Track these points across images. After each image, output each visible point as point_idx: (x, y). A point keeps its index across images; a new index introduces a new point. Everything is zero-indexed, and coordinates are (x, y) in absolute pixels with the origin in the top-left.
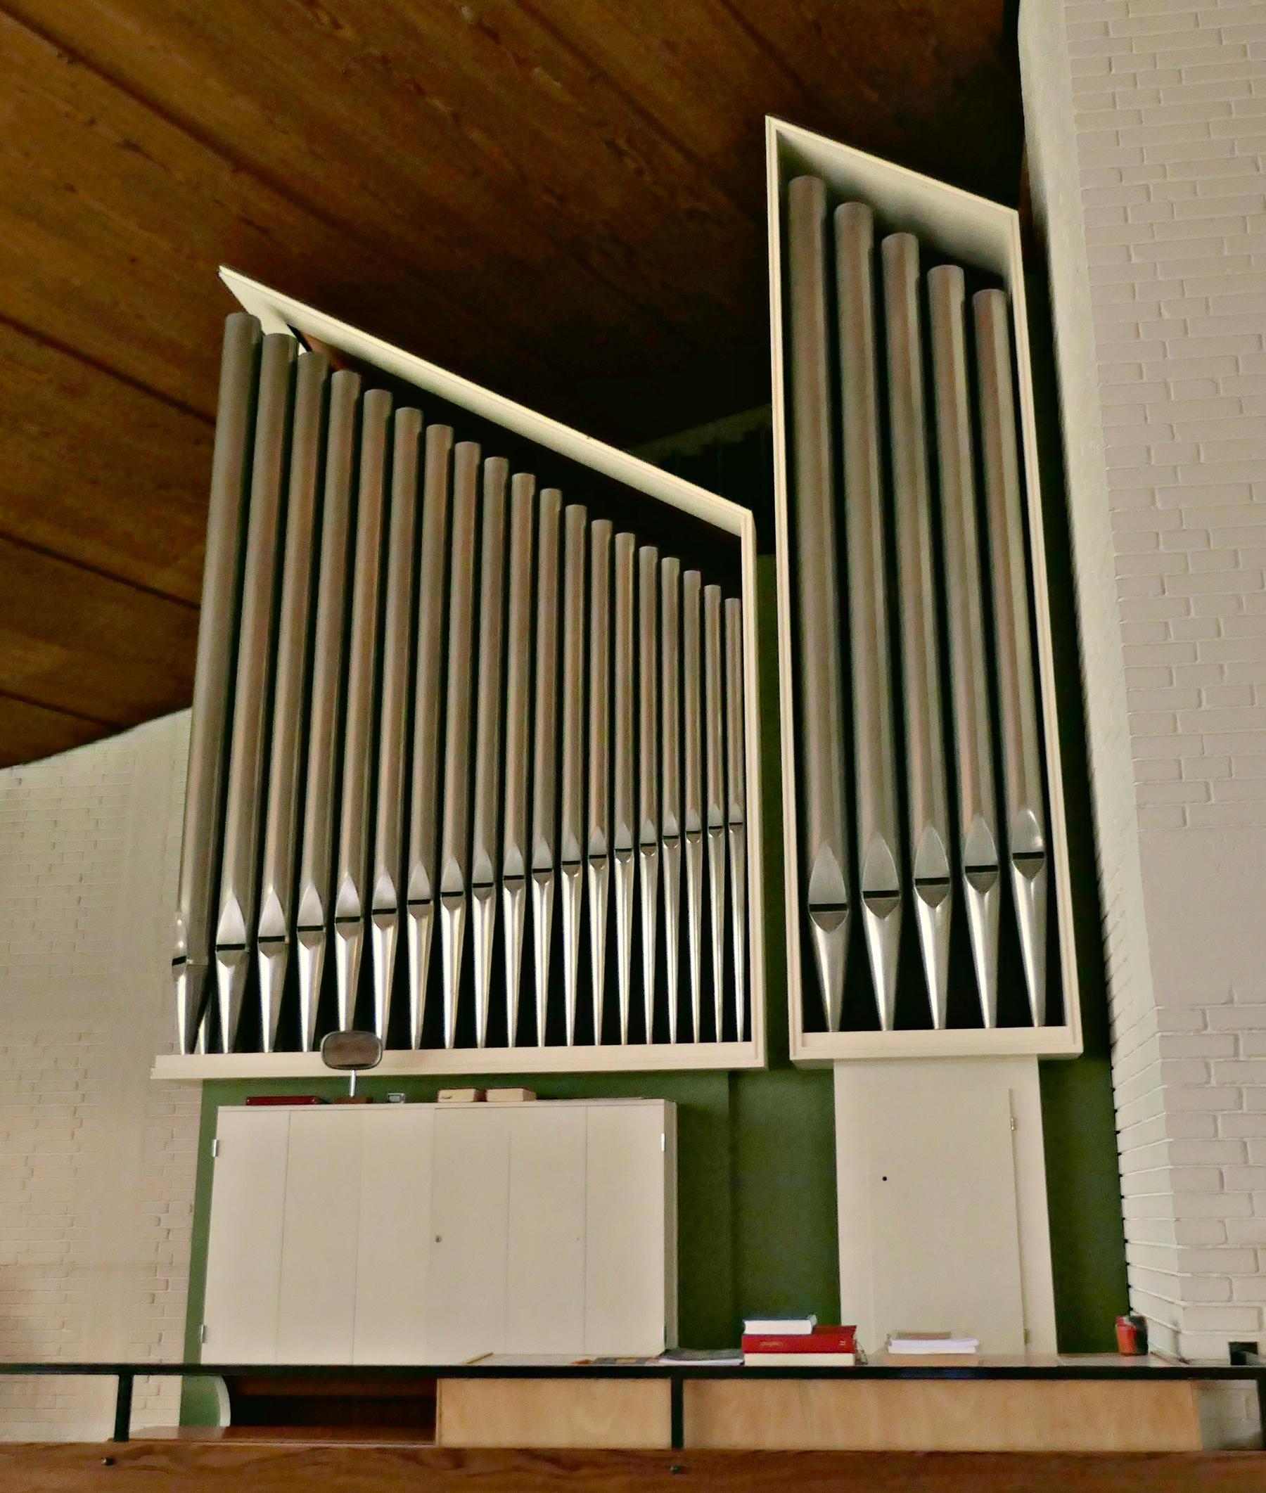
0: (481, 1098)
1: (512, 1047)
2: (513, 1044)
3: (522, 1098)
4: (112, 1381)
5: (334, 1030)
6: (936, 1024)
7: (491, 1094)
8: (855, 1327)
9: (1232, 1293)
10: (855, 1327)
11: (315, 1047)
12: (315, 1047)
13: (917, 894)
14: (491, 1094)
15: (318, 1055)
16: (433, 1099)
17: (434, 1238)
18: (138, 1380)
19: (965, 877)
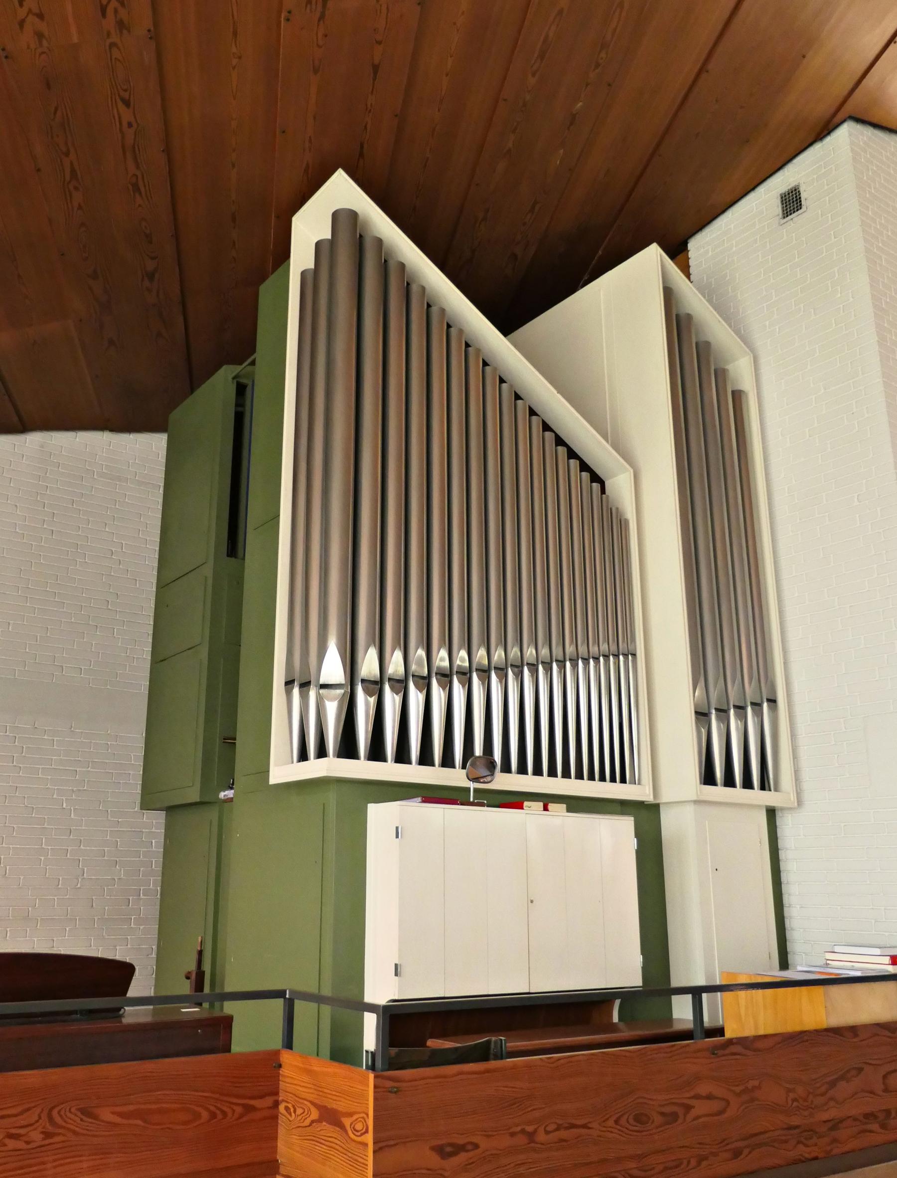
0: (546, 808)
1: (439, 767)
2: (416, 762)
3: (542, 809)
4: (689, 997)
5: (471, 757)
6: (596, 780)
7: (551, 806)
8: (292, 1050)
9: (630, 1125)
10: (292, 1050)
11: (464, 767)
12: (464, 767)
13: (411, 679)
14: (551, 806)
15: (464, 771)
16: (519, 806)
17: (534, 902)
18: (704, 996)
19: (455, 676)
